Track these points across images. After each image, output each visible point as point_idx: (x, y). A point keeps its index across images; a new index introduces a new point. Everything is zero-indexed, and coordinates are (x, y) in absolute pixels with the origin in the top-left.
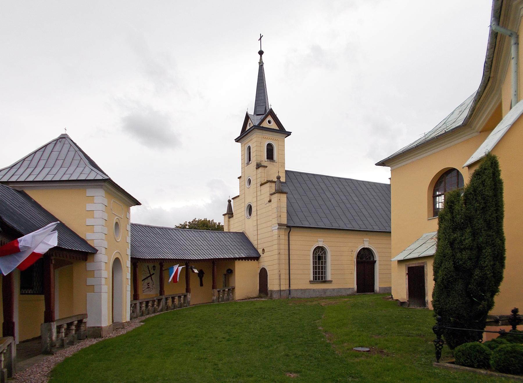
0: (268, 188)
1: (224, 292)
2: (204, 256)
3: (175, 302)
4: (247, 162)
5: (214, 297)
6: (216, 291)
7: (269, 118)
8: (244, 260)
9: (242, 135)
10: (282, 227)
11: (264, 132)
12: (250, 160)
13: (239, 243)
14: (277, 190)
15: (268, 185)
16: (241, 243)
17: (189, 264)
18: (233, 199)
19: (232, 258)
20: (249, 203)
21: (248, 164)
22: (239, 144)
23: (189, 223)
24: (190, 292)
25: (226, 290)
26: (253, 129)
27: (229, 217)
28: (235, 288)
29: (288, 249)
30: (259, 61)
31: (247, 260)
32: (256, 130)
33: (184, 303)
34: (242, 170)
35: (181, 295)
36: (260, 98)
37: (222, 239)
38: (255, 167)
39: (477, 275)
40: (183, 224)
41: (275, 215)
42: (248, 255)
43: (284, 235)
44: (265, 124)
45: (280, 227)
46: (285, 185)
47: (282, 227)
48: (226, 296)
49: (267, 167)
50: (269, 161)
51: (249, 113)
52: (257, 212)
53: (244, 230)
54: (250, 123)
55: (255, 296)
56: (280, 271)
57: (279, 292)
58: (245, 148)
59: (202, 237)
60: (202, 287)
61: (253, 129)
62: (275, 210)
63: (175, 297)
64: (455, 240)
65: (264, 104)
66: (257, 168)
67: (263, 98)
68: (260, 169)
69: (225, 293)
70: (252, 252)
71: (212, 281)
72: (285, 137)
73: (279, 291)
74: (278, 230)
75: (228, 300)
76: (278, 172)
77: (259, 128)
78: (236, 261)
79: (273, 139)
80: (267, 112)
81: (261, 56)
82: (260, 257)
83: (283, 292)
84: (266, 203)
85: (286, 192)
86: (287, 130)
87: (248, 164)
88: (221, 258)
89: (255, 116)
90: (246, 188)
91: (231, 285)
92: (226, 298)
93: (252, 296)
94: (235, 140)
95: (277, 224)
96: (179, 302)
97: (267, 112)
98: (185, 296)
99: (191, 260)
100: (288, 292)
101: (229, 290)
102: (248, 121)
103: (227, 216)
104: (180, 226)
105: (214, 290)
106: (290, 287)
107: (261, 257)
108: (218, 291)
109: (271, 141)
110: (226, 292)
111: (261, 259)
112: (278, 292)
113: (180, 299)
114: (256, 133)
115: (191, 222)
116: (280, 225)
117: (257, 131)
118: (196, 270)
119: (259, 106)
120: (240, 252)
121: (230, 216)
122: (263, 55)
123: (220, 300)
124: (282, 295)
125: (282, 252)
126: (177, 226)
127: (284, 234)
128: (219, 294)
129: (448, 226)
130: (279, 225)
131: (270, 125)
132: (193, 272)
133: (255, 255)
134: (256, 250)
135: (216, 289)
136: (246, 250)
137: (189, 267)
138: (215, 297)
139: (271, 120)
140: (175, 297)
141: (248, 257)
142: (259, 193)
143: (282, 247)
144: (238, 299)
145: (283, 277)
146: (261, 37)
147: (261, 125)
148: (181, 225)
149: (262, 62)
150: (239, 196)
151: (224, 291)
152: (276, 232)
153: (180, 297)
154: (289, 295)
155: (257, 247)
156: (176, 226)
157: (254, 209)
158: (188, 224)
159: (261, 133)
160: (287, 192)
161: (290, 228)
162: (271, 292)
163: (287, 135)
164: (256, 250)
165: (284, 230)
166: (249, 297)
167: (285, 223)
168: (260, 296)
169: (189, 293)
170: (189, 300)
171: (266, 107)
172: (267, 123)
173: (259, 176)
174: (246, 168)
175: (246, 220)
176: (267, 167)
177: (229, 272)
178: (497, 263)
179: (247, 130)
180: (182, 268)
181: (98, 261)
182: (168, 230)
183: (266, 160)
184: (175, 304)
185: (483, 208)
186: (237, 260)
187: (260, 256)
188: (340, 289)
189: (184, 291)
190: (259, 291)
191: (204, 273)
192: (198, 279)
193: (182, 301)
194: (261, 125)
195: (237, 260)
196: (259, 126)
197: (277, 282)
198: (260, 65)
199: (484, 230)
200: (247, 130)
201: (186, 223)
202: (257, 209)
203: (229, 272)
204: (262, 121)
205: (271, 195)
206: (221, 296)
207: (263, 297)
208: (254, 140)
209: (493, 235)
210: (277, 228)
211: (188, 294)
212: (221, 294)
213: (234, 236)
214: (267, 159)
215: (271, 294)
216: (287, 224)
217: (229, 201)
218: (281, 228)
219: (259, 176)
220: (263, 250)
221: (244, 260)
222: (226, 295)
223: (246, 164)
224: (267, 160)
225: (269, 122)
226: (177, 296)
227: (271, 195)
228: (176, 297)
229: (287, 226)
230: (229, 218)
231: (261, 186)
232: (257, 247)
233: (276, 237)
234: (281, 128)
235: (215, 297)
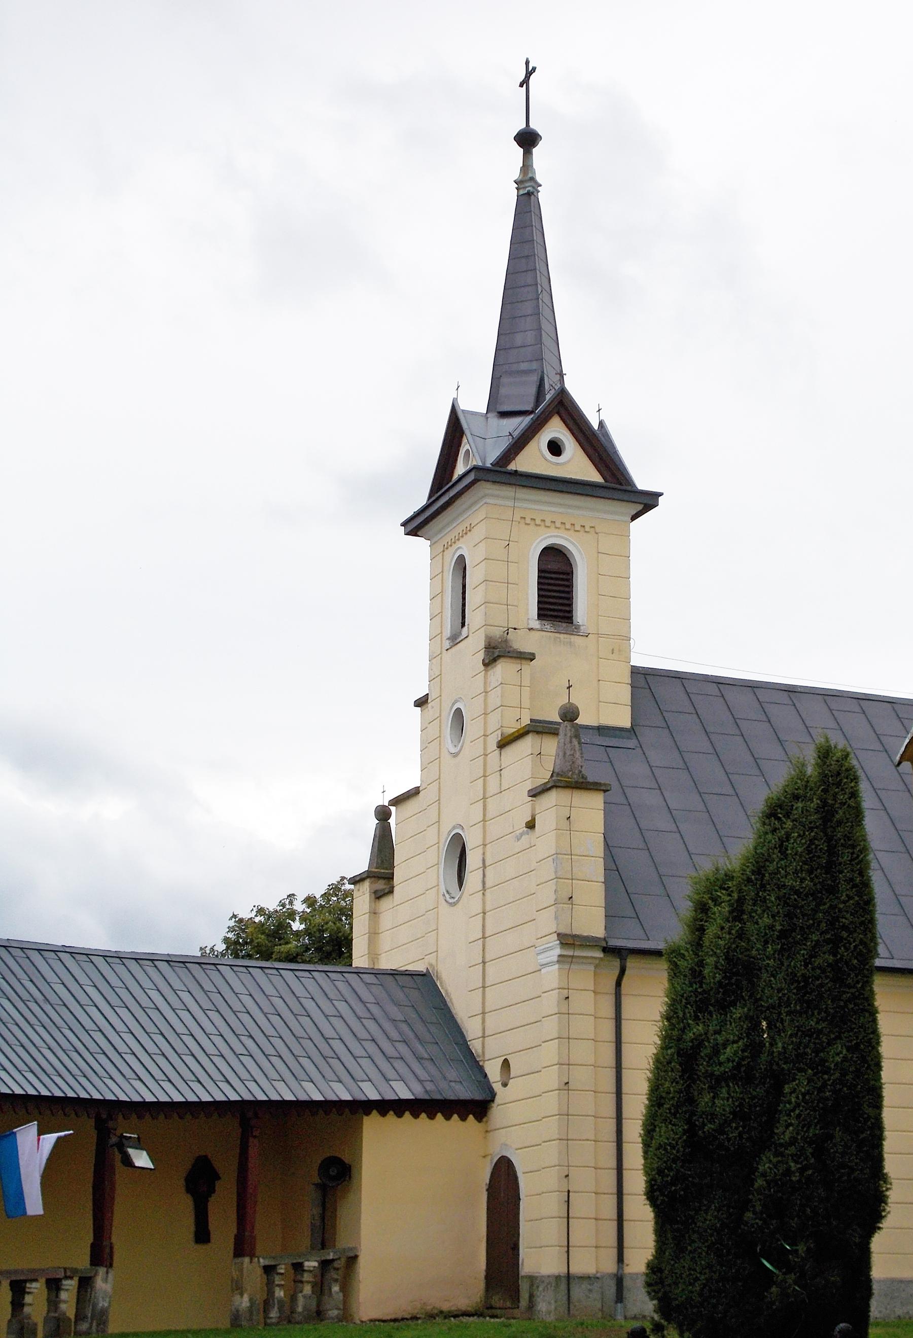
0: (528, 763)
1: (299, 1277)
2: (137, 1084)
3: (27, 1310)
4: (451, 632)
5: (242, 1295)
6: (252, 1268)
7: (556, 429)
8: (407, 1114)
9: (437, 499)
10: (576, 954)
11: (522, 493)
12: (463, 625)
13: (396, 1028)
14: (558, 774)
15: (527, 745)
16: (404, 1027)
17: (111, 1124)
18: (396, 801)
19: (341, 1102)
20: (454, 828)
21: (455, 639)
22: (421, 545)
23: (310, 901)
24: (111, 1265)
25: (306, 1264)
26: (473, 483)
27: (375, 892)
28: (356, 1257)
29: (613, 1064)
30: (516, 175)
31: (423, 1115)
32: (485, 489)
33: (80, 1316)
34: (431, 669)
35: (61, 1275)
36: (519, 339)
37: (310, 1005)
38: (481, 655)
39: (764, 1175)
40: (272, 905)
41: (547, 895)
42: (426, 1091)
43: (594, 992)
44: (526, 462)
45: (570, 953)
46: (632, 743)
47: (578, 953)
48: (304, 1297)
49: (532, 660)
50: (548, 626)
51: (463, 405)
52: (484, 875)
53: (432, 959)
54: (468, 450)
55: (463, 1302)
56: (567, 1176)
57: (563, 1286)
58: (446, 564)
59: (205, 992)
60: (202, 1248)
61: (473, 483)
62: (547, 871)
63: (25, 1281)
64: (698, 1043)
65: (535, 365)
66: (487, 661)
67: (530, 337)
68: (503, 669)
69: (302, 1282)
70: (452, 1074)
71: (234, 1216)
72: (634, 518)
73: (564, 1281)
74: (559, 969)
75: (319, 1315)
76: (569, 688)
77: (504, 478)
78: (365, 1118)
79: (568, 526)
80: (548, 397)
81: (527, 154)
82: (493, 1101)
83: (585, 1286)
84: (518, 832)
85: (600, 784)
86: (642, 483)
87: (455, 639)
88: (283, 1103)
89: (494, 421)
90: (446, 757)
91: (343, 1242)
92: (305, 1308)
93: (446, 1307)
94: (402, 525)
95: (555, 936)
96: (49, 1311)
97: (548, 397)
98: (85, 1283)
99: (118, 1103)
100: (611, 1291)
101: (325, 1264)
102: (459, 445)
103: (366, 885)
104: (257, 920)
105: (240, 1259)
106: (620, 1259)
107: (498, 1100)
108: (269, 1270)
109: (562, 533)
110: (306, 1277)
111: (497, 1113)
112: (557, 1286)
113: (57, 1296)
114: (488, 501)
115: (318, 896)
116: (568, 940)
117: (487, 491)
118: (145, 1153)
119: (511, 373)
120: (391, 1074)
121: (381, 885)
122: (535, 151)
123: (274, 1314)
124: (579, 1301)
125: (581, 1077)
126: (241, 920)
127: (593, 989)
128: (270, 1285)
129: (682, 996)
130: (561, 943)
131: (558, 464)
132: (128, 1162)
133: (464, 1092)
134: (475, 1065)
135: (252, 1256)
136: (427, 1064)
137: (114, 1140)
138: (246, 1298)
139: (562, 437)
140: (25, 1281)
141: (427, 1097)
142: (493, 784)
143: (583, 1052)
144: (371, 1317)
145: (582, 1206)
146: (529, 73)
147: (512, 467)
148: (261, 911)
149: (532, 179)
150: (415, 792)
151: (298, 1267)
152: (552, 975)
153: (54, 1285)
154: (616, 1302)
155: (480, 1051)
156: (234, 916)
157: (473, 860)
158: (299, 907)
159: (508, 498)
160: (605, 785)
161: (623, 960)
162: (532, 1285)
163: (640, 507)
164: (478, 1062)
165: (592, 968)
166: (429, 1308)
167: (598, 931)
168: (491, 1308)
169: (102, 1271)
170: (102, 1304)
171: (542, 380)
172: (543, 456)
173: (494, 699)
174: (447, 656)
175: (444, 908)
176: (531, 657)
177: (333, 1172)
178: (838, 1133)
179: (455, 477)
180: (59, 1138)
181: (498, 1127)
182: (35, 956)
183: (536, 624)
184: (29, 1317)
185: (783, 934)
186: (375, 1112)
187: (493, 1095)
188: (901, 1281)
189: (82, 1261)
190: (487, 1277)
191: (219, 1178)
192: (186, 1204)
193: (63, 1306)
194: (512, 467)
195: (375, 1112)
196: (503, 470)
197: (552, 1231)
198: (521, 192)
199: (789, 1013)
200: (455, 477)
201: (291, 903)
202: (484, 861)
203: (333, 1172)
204: (519, 444)
205: (536, 793)
206: (280, 1293)
207: (498, 1312)
208: (479, 532)
209: (820, 1032)
210: (555, 959)
211: (96, 1274)
212: (277, 1283)
213: (377, 990)
214: (541, 616)
215: (531, 1296)
216: (605, 939)
217: (383, 814)
218: (573, 957)
219: (494, 699)
220: (506, 1064)
221: (407, 1114)
222: (307, 1289)
223: (448, 639)
224: (538, 622)
225: (555, 448)
226: (36, 1280)
227: (536, 793)
228: (34, 1285)
229: (605, 950)
230: (379, 896)
231: (503, 751)
232: (480, 1051)
233: (550, 1003)
234: (613, 475)
235: (246, 1298)
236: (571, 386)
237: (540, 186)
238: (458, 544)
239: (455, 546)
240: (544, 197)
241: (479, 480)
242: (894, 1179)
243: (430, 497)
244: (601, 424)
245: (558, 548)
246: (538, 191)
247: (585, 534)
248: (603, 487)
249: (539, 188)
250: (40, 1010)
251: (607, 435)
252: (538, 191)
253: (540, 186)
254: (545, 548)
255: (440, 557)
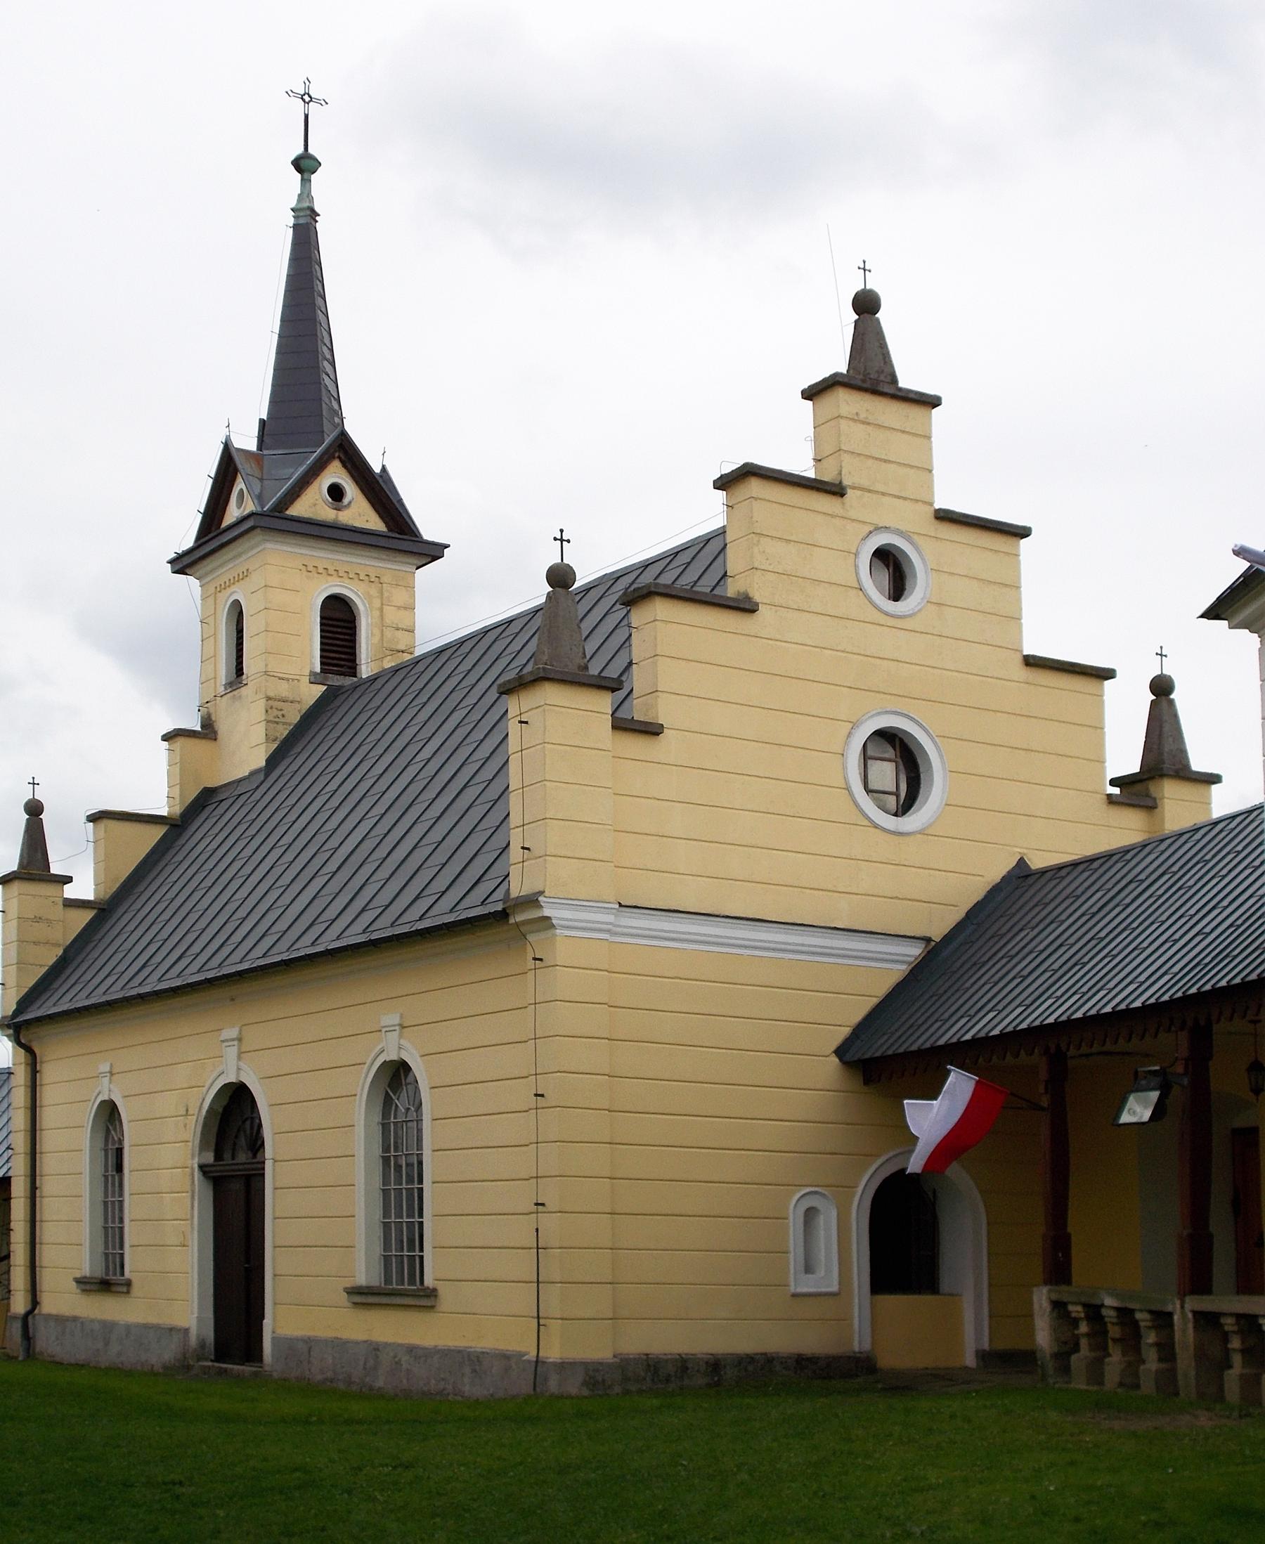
7: (335, 474)
61: (253, 528)
81: (306, 182)
109: (347, 582)
225: (336, 492)
236: (349, 428)
237: (319, 215)
238: (233, 588)
239: (229, 591)
240: (324, 228)
241: (257, 527)
242: (889, 760)
243: (198, 538)
244: (384, 469)
245: (346, 599)
246: (317, 221)
247: (316, 575)
248: (385, 536)
249: (317, 218)
250: (177, 941)
251: (389, 481)
252: (317, 221)
253: (319, 215)
254: (328, 598)
255: (211, 600)
